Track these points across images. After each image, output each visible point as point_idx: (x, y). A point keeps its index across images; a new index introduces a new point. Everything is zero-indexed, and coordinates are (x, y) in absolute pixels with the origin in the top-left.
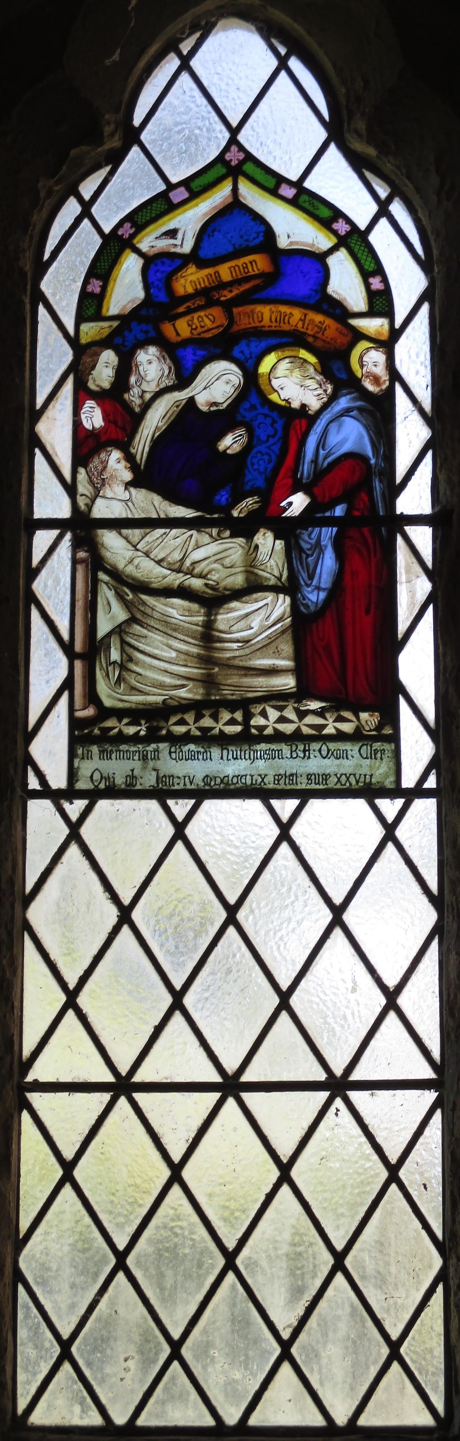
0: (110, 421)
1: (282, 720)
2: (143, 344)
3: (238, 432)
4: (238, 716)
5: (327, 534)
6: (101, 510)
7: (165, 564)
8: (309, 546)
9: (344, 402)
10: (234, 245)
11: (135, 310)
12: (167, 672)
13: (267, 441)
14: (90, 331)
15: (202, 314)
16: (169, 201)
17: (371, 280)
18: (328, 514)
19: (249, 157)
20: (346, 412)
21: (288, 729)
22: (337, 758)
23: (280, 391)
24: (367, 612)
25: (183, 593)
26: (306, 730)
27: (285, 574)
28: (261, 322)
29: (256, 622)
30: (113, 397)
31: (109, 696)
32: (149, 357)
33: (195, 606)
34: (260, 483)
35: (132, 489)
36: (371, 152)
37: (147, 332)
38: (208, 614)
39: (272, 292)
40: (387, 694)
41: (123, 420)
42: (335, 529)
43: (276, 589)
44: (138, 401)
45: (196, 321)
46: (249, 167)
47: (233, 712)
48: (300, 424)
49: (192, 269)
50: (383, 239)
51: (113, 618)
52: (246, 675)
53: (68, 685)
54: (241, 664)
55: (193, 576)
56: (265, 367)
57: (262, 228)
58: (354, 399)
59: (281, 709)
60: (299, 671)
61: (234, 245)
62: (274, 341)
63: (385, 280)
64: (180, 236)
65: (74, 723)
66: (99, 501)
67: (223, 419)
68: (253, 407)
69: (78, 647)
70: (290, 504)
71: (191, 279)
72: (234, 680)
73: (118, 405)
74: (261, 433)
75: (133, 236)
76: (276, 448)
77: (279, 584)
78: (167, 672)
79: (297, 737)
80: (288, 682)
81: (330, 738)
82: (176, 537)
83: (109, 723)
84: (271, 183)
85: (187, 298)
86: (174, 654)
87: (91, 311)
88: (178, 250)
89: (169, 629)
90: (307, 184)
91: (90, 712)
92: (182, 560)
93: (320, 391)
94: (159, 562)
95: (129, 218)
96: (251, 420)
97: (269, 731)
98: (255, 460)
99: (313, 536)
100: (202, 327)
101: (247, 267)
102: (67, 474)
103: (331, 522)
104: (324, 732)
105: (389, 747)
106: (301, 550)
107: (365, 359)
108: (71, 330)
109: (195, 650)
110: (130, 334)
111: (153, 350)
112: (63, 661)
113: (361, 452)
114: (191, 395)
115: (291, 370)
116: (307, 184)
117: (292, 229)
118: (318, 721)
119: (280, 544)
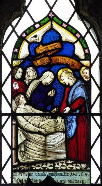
0: (20, 87)
1: (63, 166)
2: (28, 67)
3: (53, 91)
4: (52, 164)
5: (74, 117)
6: (19, 111)
7: (34, 125)
8: (70, 120)
9: (79, 83)
10: (51, 40)
11: (27, 57)
12: (35, 153)
13: (60, 93)
14: (15, 63)
15: (43, 58)
16: (35, 27)
17: (85, 50)
18: (75, 113)
19: (55, 16)
20: (79, 86)
21: (64, 168)
22: (76, 176)
23: (63, 80)
24: (84, 138)
25: (39, 133)
26: (68, 168)
27: (64, 128)
28: (58, 61)
29: (57, 140)
30: (21, 81)
31: (21, 160)
32: (31, 70)
33: (42, 136)
34: (58, 104)
35: (26, 105)
36: (87, 15)
37: (30, 63)
38: (46, 138)
39: (61, 53)
40: (87, 159)
41: (24, 87)
42: (76, 116)
43: (61, 132)
44: (28, 82)
45: (42, 61)
46: (55, 18)
47: (51, 164)
48: (67, 89)
49: (41, 46)
50: (89, 39)
51: (22, 139)
52: (54, 154)
53: (11, 157)
54: (53, 151)
55: (42, 129)
56: (59, 74)
57: (59, 36)
58: (81, 82)
59: (62, 163)
60: (67, 153)
61: (51, 40)
62: (62, 66)
63: (89, 50)
64: (38, 37)
65: (13, 166)
66: (18, 108)
67: (49, 87)
68: (56, 84)
69: (13, 147)
70: (65, 110)
71: (41, 49)
72: (51, 155)
73: (22, 83)
74: (59, 91)
75: (26, 37)
76: (62, 95)
77: (63, 131)
78: (35, 153)
79: (66, 170)
80: (64, 156)
81: (74, 170)
82: (37, 119)
83: (21, 167)
84: (60, 23)
85: (40, 54)
86: (37, 149)
87: (15, 57)
88: (37, 41)
89: (37, 142)
90: (70, 23)
91: (16, 164)
92: (39, 124)
93: (73, 80)
94: (33, 125)
95: (25, 32)
96: (56, 87)
97: (60, 168)
98: (57, 98)
99: (70, 118)
100: (44, 62)
101: (55, 46)
102: (10, 102)
103: (75, 115)
104: (73, 169)
105: (88, 173)
106: (68, 121)
107: (84, 72)
108: (10, 62)
109: (42, 148)
110: (26, 63)
111: (31, 68)
112: (10, 151)
113: (83, 96)
114: (41, 80)
115: (66, 74)
116: (70, 23)
117: (67, 36)
118: (72, 166)
119: (63, 120)
